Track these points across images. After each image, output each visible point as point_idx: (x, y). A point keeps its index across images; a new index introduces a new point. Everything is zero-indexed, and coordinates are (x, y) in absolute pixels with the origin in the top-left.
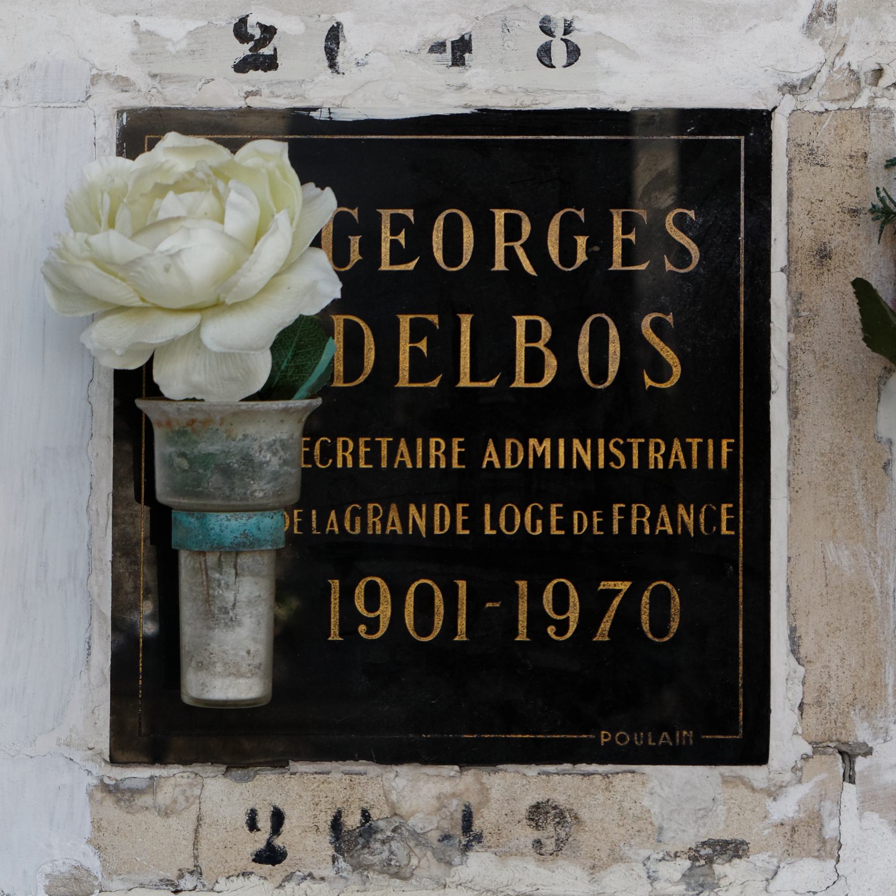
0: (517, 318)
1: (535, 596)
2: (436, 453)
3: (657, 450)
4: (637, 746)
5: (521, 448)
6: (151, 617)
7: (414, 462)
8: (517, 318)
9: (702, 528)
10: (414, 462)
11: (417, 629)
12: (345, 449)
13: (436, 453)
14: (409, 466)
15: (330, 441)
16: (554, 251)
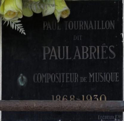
0: (43, 47)
1: (89, 57)
2: (85, 52)
3: (85, 51)
4: (113, 82)
5: (76, 37)
6: (22, 83)
7: (94, 27)
8: (43, 47)
9: (109, 74)
10: (94, 27)
11: (104, 97)
12: (85, 51)
13: (85, 52)
14: (93, 29)
15: (114, 47)
16: (69, 27)
